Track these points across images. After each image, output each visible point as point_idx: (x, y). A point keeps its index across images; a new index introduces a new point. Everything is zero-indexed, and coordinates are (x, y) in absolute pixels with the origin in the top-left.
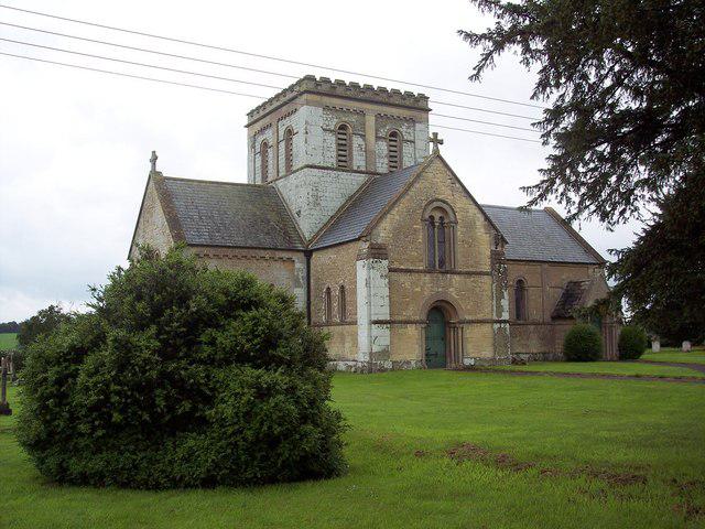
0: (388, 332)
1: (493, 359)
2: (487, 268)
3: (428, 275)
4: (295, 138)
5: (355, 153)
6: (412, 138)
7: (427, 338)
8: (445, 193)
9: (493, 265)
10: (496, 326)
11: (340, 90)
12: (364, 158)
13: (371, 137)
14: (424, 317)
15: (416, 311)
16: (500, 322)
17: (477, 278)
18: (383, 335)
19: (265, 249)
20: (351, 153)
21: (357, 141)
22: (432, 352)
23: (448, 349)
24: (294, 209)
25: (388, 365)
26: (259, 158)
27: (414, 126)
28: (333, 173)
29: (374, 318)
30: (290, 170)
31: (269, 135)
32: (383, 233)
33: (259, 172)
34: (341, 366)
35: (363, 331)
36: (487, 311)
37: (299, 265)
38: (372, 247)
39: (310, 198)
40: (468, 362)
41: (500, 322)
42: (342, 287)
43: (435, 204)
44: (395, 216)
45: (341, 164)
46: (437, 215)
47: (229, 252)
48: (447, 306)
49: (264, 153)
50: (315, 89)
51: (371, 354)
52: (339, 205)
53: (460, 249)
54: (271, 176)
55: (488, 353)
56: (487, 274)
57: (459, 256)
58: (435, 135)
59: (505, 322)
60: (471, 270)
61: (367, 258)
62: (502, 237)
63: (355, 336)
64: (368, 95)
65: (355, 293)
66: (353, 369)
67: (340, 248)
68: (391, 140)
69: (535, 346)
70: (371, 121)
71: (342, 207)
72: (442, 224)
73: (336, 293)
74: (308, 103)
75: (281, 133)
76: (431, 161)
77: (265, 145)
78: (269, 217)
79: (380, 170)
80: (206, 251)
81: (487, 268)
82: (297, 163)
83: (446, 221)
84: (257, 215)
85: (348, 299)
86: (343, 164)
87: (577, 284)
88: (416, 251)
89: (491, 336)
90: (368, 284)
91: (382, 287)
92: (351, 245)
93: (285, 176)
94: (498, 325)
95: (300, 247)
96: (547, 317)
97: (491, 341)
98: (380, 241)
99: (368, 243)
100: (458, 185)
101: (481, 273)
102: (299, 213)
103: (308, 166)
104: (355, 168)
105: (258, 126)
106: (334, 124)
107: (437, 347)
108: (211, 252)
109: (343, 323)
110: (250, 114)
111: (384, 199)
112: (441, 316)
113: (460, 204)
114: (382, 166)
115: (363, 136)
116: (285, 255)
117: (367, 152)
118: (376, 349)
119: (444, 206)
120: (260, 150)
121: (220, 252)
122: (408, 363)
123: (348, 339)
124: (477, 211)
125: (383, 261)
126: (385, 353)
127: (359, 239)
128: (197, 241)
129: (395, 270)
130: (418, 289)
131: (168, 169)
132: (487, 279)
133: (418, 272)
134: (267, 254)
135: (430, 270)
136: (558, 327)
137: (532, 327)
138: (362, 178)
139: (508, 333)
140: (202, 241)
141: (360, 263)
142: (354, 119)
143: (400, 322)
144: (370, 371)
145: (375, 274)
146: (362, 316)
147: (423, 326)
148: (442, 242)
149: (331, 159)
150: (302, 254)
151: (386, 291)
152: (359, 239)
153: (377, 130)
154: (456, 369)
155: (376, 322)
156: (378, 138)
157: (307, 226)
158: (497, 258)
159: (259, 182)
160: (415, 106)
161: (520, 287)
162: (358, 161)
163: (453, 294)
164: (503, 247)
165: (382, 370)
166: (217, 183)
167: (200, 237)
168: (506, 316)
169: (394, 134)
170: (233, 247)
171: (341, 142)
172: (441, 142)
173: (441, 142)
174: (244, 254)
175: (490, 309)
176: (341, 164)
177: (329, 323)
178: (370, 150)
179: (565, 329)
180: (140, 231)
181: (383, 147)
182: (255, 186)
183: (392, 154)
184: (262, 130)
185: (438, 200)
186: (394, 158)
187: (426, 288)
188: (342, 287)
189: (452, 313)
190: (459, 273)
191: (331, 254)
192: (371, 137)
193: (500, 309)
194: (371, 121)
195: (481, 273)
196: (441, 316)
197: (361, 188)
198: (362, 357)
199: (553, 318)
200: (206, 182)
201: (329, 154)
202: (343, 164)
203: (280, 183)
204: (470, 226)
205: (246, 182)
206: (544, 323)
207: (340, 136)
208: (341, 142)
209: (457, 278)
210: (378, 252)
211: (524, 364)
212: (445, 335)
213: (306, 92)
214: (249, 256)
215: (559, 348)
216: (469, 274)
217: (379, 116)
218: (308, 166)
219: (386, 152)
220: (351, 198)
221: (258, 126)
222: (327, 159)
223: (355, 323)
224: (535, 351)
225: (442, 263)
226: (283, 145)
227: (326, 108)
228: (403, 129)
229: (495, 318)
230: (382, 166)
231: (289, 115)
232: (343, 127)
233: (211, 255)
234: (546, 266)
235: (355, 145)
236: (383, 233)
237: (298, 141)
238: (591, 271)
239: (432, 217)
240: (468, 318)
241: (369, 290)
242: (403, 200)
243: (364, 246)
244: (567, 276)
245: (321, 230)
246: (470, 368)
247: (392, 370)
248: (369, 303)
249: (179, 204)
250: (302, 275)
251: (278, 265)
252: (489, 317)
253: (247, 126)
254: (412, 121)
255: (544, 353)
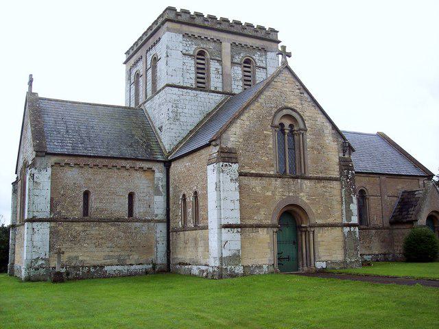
0: (238, 236)
1: (344, 262)
2: (336, 174)
3: (279, 180)
4: (159, 64)
5: (212, 76)
6: (264, 65)
7: (279, 242)
8: (295, 102)
9: (341, 174)
10: (347, 229)
11: (198, 21)
12: (220, 80)
13: (227, 61)
14: (276, 222)
15: (267, 215)
16: (350, 226)
17: (326, 183)
18: (234, 240)
19: (126, 159)
20: (209, 77)
21: (214, 65)
22: (284, 255)
23: (300, 253)
24: (157, 125)
25: (239, 270)
26: (133, 87)
27: (266, 55)
28: (192, 93)
29: (224, 222)
30: (155, 92)
31: (140, 67)
32: (233, 138)
33: (133, 98)
34: (195, 270)
35: (213, 235)
36: (337, 216)
37: (159, 174)
38: (222, 151)
39: (173, 116)
40: (320, 265)
41: (350, 226)
42: (196, 193)
43: (285, 112)
44: (245, 121)
45: (200, 85)
46: (287, 123)
47: (90, 161)
48: (297, 210)
49: (137, 83)
50: (173, 18)
51: (221, 259)
52: (197, 121)
53: (310, 155)
54: (142, 99)
55: (338, 256)
56: (336, 179)
57: (309, 162)
58: (284, 48)
59: (354, 225)
60: (320, 175)
61: (217, 162)
62: (350, 146)
63: (206, 240)
64: (223, 26)
65: (206, 198)
66: (205, 274)
67: (194, 155)
68: (245, 67)
69: (376, 249)
70: (226, 48)
71: (201, 122)
72: (292, 131)
73: (190, 199)
74: (168, 30)
75: (149, 62)
76: (280, 72)
77: (138, 75)
78: (134, 132)
79: (236, 92)
80: (67, 160)
81: (336, 174)
82: (160, 85)
83: (295, 128)
84: (128, 141)
85: (201, 204)
86: (202, 85)
87: (412, 193)
88: (267, 155)
89: (341, 239)
90: (218, 188)
91: (232, 190)
92: (203, 151)
93: (151, 98)
94: (348, 229)
95: (160, 158)
96: (387, 224)
97: (341, 244)
98: (230, 145)
99: (218, 148)
100: (306, 95)
101: (331, 179)
102: (160, 129)
103: (168, 85)
104: (213, 89)
105: (132, 61)
106: (193, 49)
107: (290, 251)
108: (72, 161)
109: (196, 228)
110: (127, 53)
111: (234, 110)
112: (292, 221)
113: (309, 112)
114: (237, 88)
115: (220, 61)
116: (146, 165)
117: (223, 75)
118: (226, 254)
119: (294, 114)
120: (134, 80)
121: (81, 161)
122: (260, 267)
123: (201, 243)
124: (324, 120)
125: (233, 165)
126: (235, 258)
127: (208, 145)
128: (59, 151)
129: (246, 175)
130: (269, 194)
131: (42, 91)
132: (336, 185)
133: (270, 176)
134: (128, 164)
135: (281, 175)
136: (396, 231)
137: (374, 231)
138: (218, 98)
139: (357, 236)
140: (65, 151)
141: (210, 167)
142: (211, 46)
143: (252, 226)
144: (221, 277)
145: (225, 178)
146: (213, 220)
147: (275, 230)
148: (292, 148)
149: (190, 79)
150: (162, 165)
151: (237, 195)
152: (208, 145)
153: (232, 57)
154: (308, 274)
155: (226, 226)
156: (233, 63)
157: (168, 140)
158: (345, 165)
159: (133, 105)
160: (267, 37)
161: (362, 196)
162: (215, 82)
163: (304, 199)
164: (350, 154)
165: (233, 275)
166: (90, 104)
167: (62, 147)
168: (355, 220)
169: (247, 61)
170: (94, 157)
171: (200, 66)
172: (289, 55)
173: (289, 55)
174: (105, 163)
175: (339, 213)
176: (200, 85)
177: (184, 229)
178: (226, 73)
179: (404, 232)
180: (22, 147)
181: (238, 72)
182: (129, 108)
183: (247, 78)
184: (135, 64)
185: (287, 108)
186: (248, 81)
187: (277, 193)
188: (196, 193)
189: (303, 217)
190: (309, 179)
191: (186, 162)
192: (227, 61)
193: (349, 212)
194: (226, 48)
195: (331, 179)
196: (292, 221)
197: (218, 106)
198: (214, 263)
199: (392, 223)
200: (80, 103)
201: (188, 76)
202: (202, 85)
203: (147, 105)
204: (319, 134)
205: (123, 104)
206: (383, 228)
207: (199, 61)
208: (200, 66)
209: (307, 182)
210: (228, 156)
211: (369, 265)
212: (297, 240)
213: (167, 20)
214: (110, 166)
215: (399, 249)
216: (319, 179)
217: (234, 45)
218: (168, 85)
219: (241, 76)
220: (209, 114)
221: (132, 61)
222: (186, 80)
223: (206, 228)
224: (377, 253)
225: (293, 169)
226: (150, 72)
227: (186, 35)
228: (256, 57)
229: (345, 222)
230: (237, 88)
231: (155, 44)
232: (201, 53)
233: (72, 164)
234: (383, 178)
235: (212, 69)
236: (233, 138)
237: (161, 65)
238: (421, 183)
239: (282, 125)
240: (319, 222)
241: (219, 192)
242: (252, 107)
243: (214, 150)
244: (401, 187)
245: (180, 143)
246: (322, 273)
247: (244, 275)
248: (219, 207)
249: (49, 120)
250: (162, 184)
251: (138, 174)
252: (339, 221)
253: (125, 63)
254: (264, 50)
255: (385, 254)
